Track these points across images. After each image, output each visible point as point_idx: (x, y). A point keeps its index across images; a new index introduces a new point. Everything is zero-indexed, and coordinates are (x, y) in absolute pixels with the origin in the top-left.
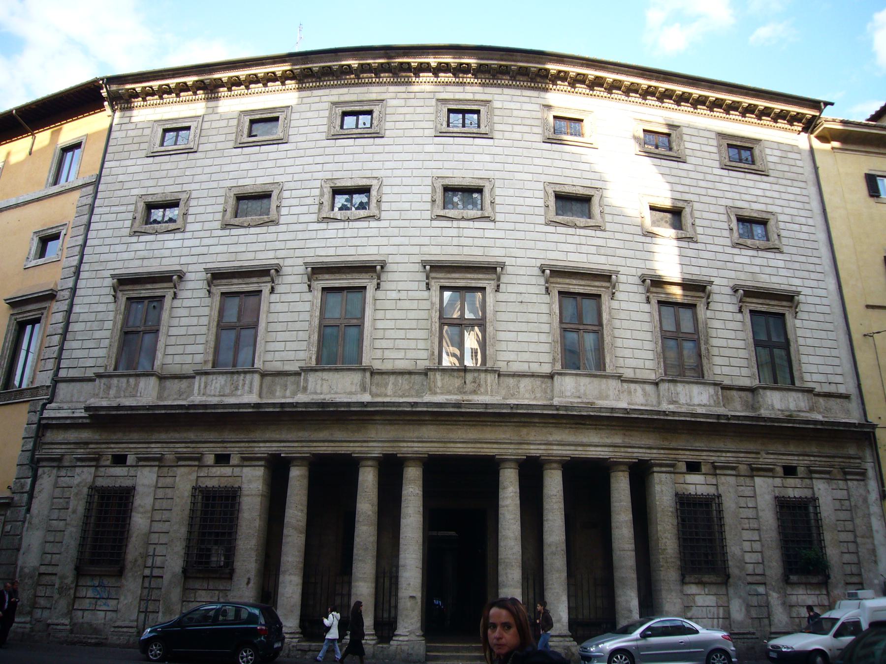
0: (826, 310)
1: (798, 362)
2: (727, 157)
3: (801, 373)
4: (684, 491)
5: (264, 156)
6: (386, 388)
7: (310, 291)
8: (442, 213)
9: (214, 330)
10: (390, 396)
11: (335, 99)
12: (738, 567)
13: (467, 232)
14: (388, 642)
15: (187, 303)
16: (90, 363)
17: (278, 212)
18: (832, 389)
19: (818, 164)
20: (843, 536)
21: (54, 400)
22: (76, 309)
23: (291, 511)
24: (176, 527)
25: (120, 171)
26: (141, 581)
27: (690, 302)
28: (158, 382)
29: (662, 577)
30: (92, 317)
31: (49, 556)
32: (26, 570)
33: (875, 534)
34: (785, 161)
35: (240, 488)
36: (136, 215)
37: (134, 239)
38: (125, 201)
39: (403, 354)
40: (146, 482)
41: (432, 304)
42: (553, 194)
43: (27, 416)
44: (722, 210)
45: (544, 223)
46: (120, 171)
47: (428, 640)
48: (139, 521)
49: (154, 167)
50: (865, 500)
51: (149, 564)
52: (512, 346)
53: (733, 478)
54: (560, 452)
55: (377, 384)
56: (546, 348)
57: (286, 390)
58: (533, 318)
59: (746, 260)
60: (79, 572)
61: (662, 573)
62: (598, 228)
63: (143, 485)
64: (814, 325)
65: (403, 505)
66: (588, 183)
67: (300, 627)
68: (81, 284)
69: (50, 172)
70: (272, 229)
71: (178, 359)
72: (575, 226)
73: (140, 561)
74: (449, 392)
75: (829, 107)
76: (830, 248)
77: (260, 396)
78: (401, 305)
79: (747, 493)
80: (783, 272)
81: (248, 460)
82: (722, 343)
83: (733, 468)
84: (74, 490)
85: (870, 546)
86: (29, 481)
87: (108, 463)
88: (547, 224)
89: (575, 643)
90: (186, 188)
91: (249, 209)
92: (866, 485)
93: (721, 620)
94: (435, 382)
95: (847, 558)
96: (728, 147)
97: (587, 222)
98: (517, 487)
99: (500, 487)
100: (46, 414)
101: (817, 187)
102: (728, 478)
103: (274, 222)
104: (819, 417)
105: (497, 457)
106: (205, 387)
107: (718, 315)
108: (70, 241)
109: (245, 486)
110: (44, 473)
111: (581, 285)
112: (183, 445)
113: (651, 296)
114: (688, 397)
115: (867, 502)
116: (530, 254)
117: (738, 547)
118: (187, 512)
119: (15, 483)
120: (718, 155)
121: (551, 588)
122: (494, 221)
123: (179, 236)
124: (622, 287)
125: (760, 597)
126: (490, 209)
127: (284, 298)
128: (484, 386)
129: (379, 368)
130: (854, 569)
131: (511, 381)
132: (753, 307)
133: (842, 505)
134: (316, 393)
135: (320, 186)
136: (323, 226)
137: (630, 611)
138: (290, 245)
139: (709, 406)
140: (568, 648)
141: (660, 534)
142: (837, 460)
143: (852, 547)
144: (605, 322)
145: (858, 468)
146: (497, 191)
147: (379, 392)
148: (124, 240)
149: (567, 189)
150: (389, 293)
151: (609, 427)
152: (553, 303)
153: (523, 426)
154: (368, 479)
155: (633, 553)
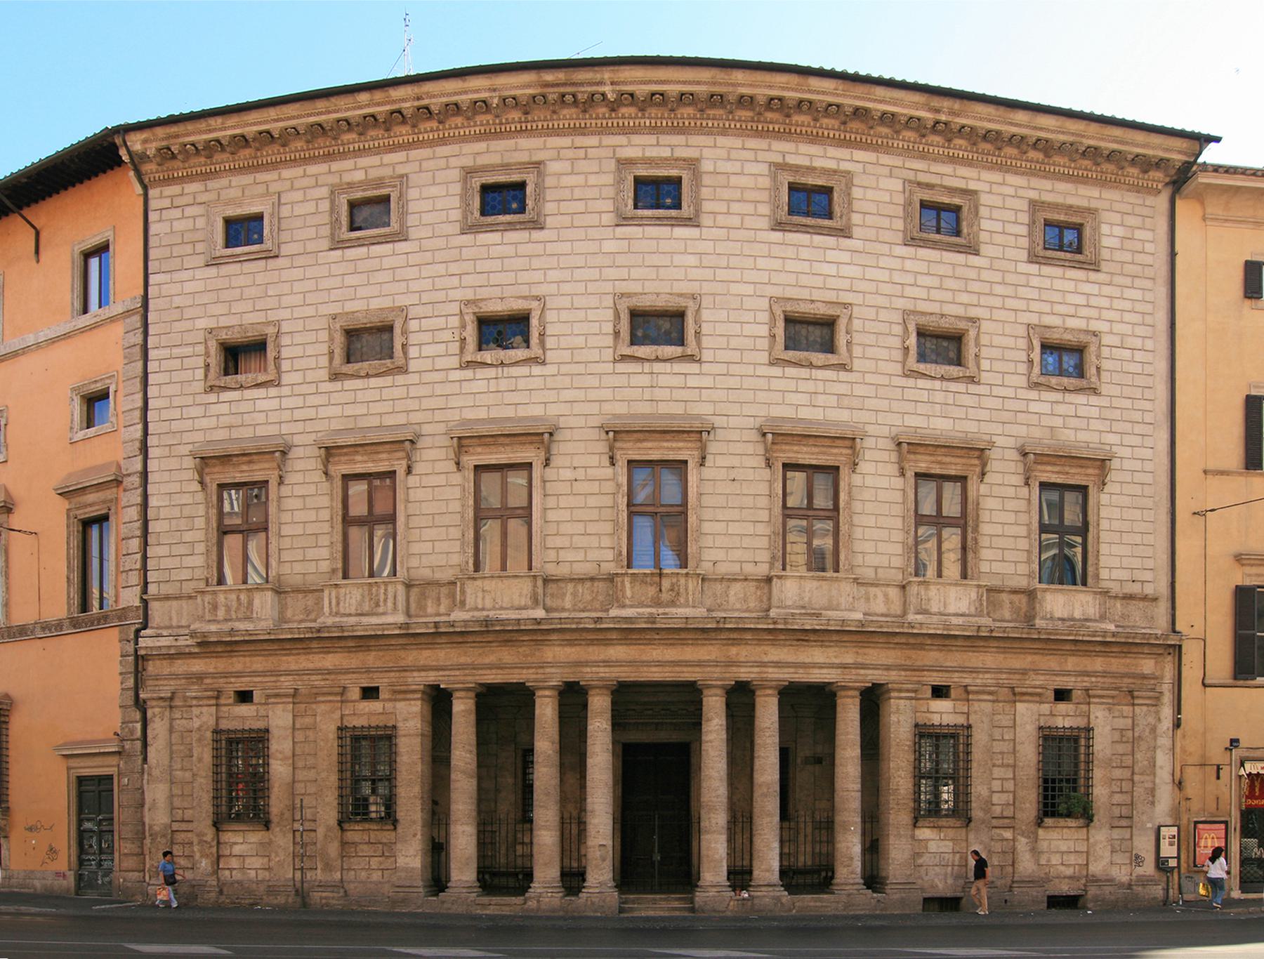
0: (1148, 478)
1: (1095, 553)
2: (1041, 243)
3: (1097, 569)
4: (926, 721)
5: (375, 264)
6: (563, 600)
7: (459, 470)
8: (628, 351)
9: (339, 527)
10: (568, 610)
11: (468, 162)
12: (984, 810)
13: (664, 381)
14: (577, 895)
15: (299, 491)
16: (185, 575)
17: (405, 353)
18: (1135, 589)
19: (1178, 247)
20: (1118, 773)
21: (150, 625)
22: (153, 502)
23: (457, 753)
24: (324, 775)
25: (175, 289)
26: (291, 835)
27: (959, 473)
28: (276, 599)
29: (891, 821)
30: (176, 512)
31: (180, 812)
32: (156, 828)
33: (1158, 771)
34: (1128, 245)
35: (394, 727)
36: (208, 360)
37: (212, 397)
38: (189, 338)
39: (583, 555)
40: (281, 723)
41: (619, 486)
42: (782, 317)
43: (118, 645)
44: (1022, 331)
45: (767, 362)
46: (175, 289)
47: (621, 892)
48: (279, 770)
49: (221, 283)
50: (1153, 730)
51: (298, 817)
52: (720, 541)
53: (990, 704)
54: (777, 676)
55: (552, 595)
56: (764, 542)
57: (439, 605)
58: (748, 501)
59: (1045, 408)
60: (217, 825)
61: (892, 817)
62: (843, 367)
63: (277, 727)
64: (1126, 501)
65: (589, 741)
66: (831, 296)
67: (478, 880)
68: (152, 466)
69: (73, 291)
70: (400, 379)
71: (298, 568)
72: (811, 366)
73: (287, 815)
74: (641, 605)
75: (1212, 145)
76: (1169, 385)
77: (408, 615)
78: (578, 487)
79: (1005, 723)
80: (1095, 425)
81: (401, 693)
82: (998, 529)
83: (990, 693)
84: (195, 736)
85: (1149, 785)
86: (139, 726)
87: (231, 701)
88: (771, 364)
89: (786, 893)
90: (272, 316)
91: (365, 349)
92: (1157, 713)
93: (956, 868)
94: (623, 590)
95: (1118, 798)
96: (1045, 225)
97: (828, 359)
98: (724, 718)
99: (704, 719)
100: (142, 642)
101: (1169, 286)
102: (983, 705)
103: (403, 370)
104: (1112, 627)
105: (700, 683)
106: (338, 604)
107: (996, 491)
108: (124, 403)
109: (400, 725)
110: (154, 715)
111: (813, 454)
112: (320, 677)
113: (907, 466)
114: (942, 604)
115: (1155, 732)
116: (748, 410)
117: (985, 787)
118: (335, 758)
119: (122, 729)
120: (1027, 239)
121: (760, 834)
122: (699, 361)
123: (273, 391)
124: (868, 455)
125: (1005, 843)
126: (694, 343)
127: (426, 481)
128: (684, 596)
129: (554, 573)
130: (1125, 811)
131: (719, 588)
132: (1046, 477)
133: (1122, 736)
134: (476, 609)
135: (458, 312)
136: (468, 374)
137: (851, 859)
138: (426, 404)
139: (968, 615)
140: (778, 899)
141: (892, 771)
142: (1126, 680)
143: (1126, 786)
144: (842, 504)
145: (1153, 690)
146: (706, 315)
147: (554, 605)
148: (199, 399)
149: (804, 308)
150: (562, 470)
151: (839, 644)
152: (775, 480)
153: (733, 645)
154: (546, 711)
155: (859, 794)
